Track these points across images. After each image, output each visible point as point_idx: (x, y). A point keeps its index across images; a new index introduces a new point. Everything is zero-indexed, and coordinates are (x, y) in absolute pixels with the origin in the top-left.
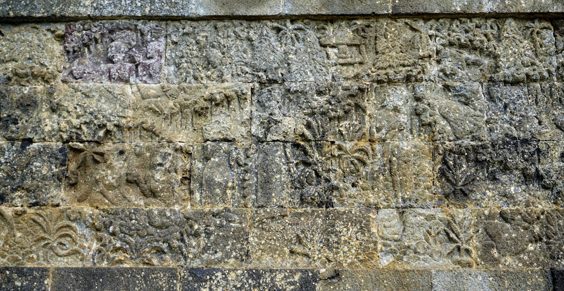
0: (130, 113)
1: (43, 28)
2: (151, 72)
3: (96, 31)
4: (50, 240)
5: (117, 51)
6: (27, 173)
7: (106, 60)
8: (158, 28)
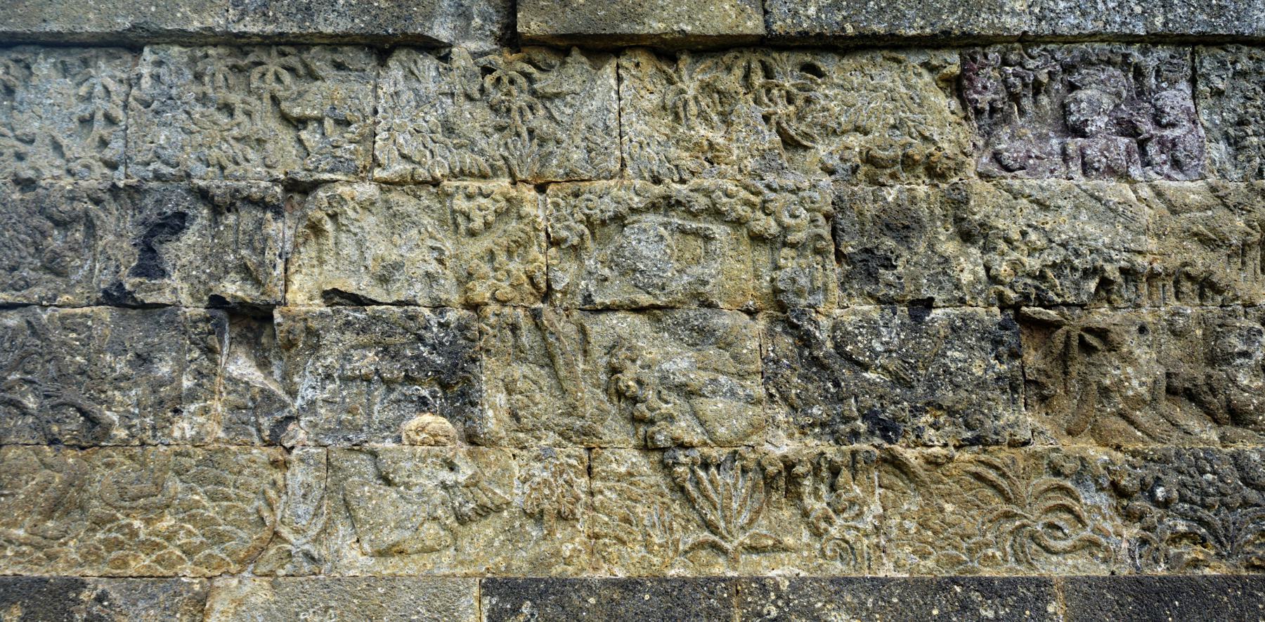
0: (1151, 244)
1: (914, 60)
2: (1180, 155)
3: (1038, 66)
4: (1026, 517)
5: (1094, 111)
6: (937, 375)
7: (1061, 131)
8: (1175, 61)
